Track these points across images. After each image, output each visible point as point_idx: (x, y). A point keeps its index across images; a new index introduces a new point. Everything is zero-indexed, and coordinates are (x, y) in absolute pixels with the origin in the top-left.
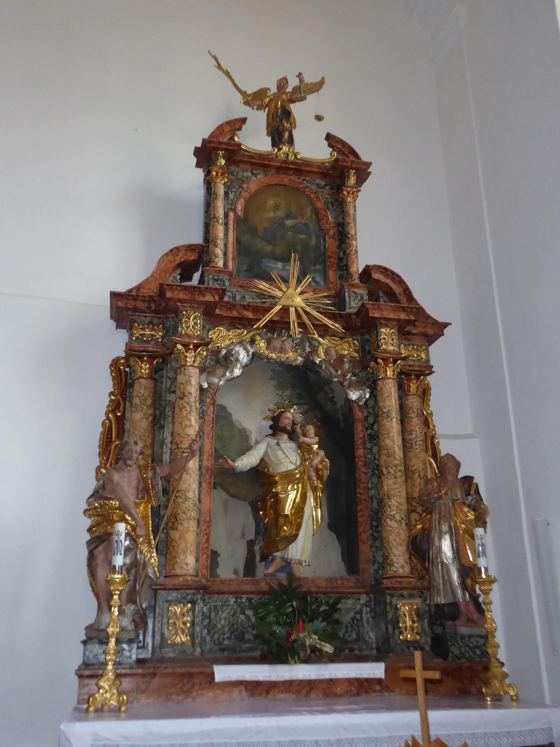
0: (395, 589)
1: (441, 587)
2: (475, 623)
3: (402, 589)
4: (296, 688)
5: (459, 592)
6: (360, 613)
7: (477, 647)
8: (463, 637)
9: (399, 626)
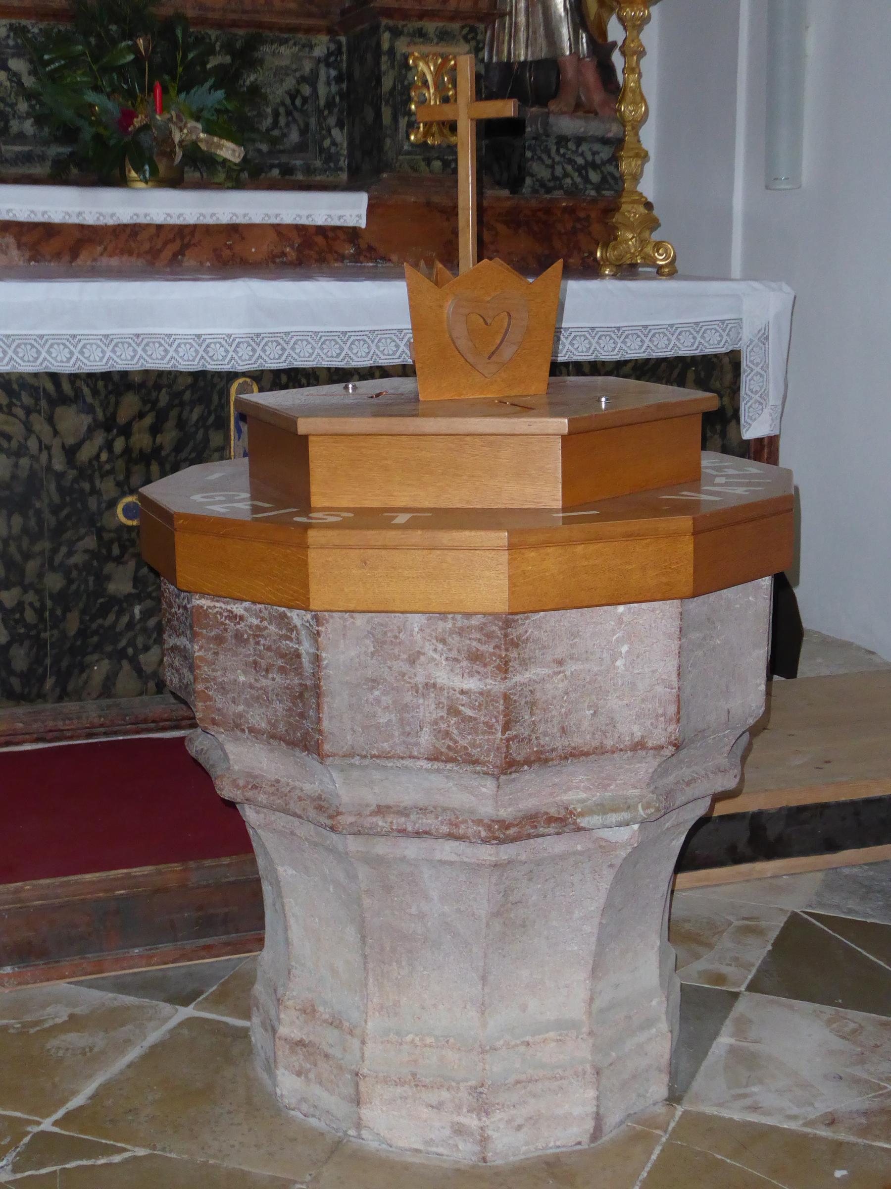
0: (404, 15)
1: (522, 19)
2: (596, 114)
3: (422, 15)
4: (147, 246)
5: (565, 32)
6: (312, 80)
7: (594, 166)
8: (562, 140)
9: (410, 109)
